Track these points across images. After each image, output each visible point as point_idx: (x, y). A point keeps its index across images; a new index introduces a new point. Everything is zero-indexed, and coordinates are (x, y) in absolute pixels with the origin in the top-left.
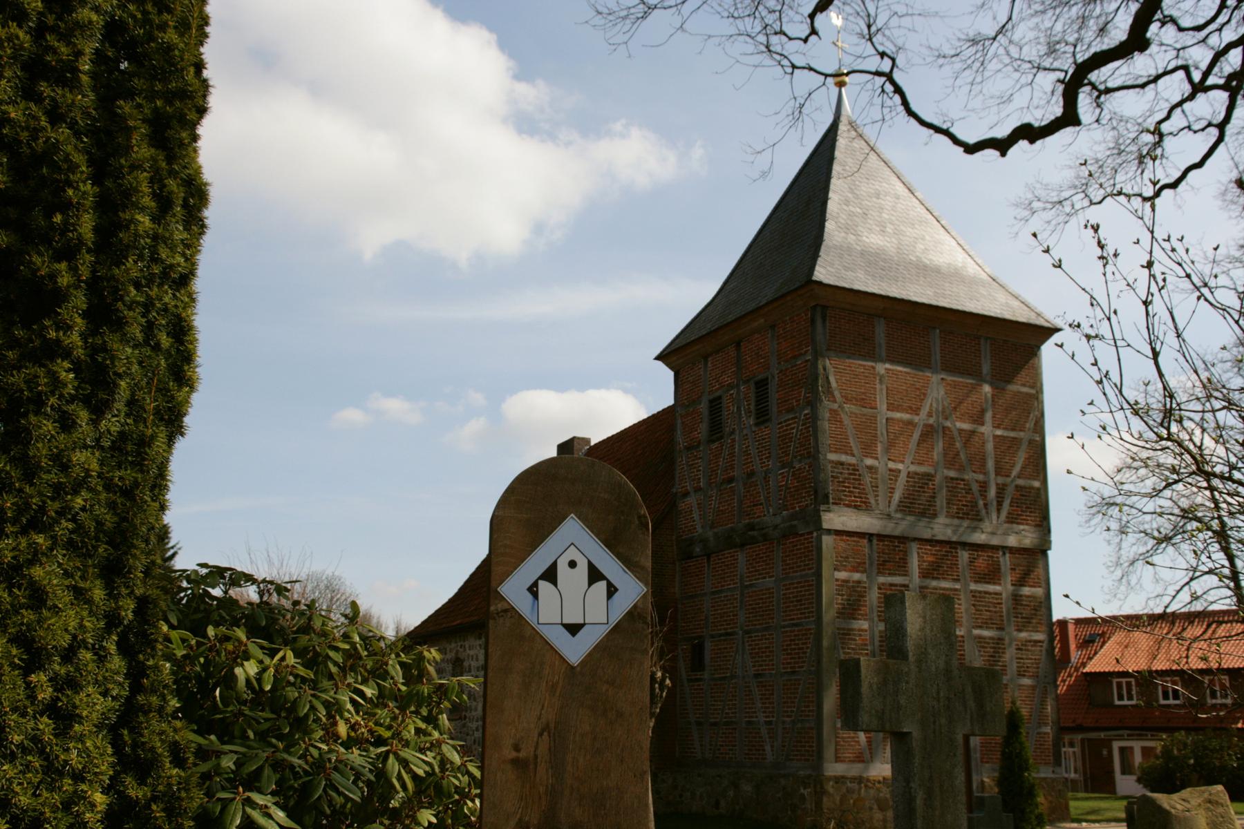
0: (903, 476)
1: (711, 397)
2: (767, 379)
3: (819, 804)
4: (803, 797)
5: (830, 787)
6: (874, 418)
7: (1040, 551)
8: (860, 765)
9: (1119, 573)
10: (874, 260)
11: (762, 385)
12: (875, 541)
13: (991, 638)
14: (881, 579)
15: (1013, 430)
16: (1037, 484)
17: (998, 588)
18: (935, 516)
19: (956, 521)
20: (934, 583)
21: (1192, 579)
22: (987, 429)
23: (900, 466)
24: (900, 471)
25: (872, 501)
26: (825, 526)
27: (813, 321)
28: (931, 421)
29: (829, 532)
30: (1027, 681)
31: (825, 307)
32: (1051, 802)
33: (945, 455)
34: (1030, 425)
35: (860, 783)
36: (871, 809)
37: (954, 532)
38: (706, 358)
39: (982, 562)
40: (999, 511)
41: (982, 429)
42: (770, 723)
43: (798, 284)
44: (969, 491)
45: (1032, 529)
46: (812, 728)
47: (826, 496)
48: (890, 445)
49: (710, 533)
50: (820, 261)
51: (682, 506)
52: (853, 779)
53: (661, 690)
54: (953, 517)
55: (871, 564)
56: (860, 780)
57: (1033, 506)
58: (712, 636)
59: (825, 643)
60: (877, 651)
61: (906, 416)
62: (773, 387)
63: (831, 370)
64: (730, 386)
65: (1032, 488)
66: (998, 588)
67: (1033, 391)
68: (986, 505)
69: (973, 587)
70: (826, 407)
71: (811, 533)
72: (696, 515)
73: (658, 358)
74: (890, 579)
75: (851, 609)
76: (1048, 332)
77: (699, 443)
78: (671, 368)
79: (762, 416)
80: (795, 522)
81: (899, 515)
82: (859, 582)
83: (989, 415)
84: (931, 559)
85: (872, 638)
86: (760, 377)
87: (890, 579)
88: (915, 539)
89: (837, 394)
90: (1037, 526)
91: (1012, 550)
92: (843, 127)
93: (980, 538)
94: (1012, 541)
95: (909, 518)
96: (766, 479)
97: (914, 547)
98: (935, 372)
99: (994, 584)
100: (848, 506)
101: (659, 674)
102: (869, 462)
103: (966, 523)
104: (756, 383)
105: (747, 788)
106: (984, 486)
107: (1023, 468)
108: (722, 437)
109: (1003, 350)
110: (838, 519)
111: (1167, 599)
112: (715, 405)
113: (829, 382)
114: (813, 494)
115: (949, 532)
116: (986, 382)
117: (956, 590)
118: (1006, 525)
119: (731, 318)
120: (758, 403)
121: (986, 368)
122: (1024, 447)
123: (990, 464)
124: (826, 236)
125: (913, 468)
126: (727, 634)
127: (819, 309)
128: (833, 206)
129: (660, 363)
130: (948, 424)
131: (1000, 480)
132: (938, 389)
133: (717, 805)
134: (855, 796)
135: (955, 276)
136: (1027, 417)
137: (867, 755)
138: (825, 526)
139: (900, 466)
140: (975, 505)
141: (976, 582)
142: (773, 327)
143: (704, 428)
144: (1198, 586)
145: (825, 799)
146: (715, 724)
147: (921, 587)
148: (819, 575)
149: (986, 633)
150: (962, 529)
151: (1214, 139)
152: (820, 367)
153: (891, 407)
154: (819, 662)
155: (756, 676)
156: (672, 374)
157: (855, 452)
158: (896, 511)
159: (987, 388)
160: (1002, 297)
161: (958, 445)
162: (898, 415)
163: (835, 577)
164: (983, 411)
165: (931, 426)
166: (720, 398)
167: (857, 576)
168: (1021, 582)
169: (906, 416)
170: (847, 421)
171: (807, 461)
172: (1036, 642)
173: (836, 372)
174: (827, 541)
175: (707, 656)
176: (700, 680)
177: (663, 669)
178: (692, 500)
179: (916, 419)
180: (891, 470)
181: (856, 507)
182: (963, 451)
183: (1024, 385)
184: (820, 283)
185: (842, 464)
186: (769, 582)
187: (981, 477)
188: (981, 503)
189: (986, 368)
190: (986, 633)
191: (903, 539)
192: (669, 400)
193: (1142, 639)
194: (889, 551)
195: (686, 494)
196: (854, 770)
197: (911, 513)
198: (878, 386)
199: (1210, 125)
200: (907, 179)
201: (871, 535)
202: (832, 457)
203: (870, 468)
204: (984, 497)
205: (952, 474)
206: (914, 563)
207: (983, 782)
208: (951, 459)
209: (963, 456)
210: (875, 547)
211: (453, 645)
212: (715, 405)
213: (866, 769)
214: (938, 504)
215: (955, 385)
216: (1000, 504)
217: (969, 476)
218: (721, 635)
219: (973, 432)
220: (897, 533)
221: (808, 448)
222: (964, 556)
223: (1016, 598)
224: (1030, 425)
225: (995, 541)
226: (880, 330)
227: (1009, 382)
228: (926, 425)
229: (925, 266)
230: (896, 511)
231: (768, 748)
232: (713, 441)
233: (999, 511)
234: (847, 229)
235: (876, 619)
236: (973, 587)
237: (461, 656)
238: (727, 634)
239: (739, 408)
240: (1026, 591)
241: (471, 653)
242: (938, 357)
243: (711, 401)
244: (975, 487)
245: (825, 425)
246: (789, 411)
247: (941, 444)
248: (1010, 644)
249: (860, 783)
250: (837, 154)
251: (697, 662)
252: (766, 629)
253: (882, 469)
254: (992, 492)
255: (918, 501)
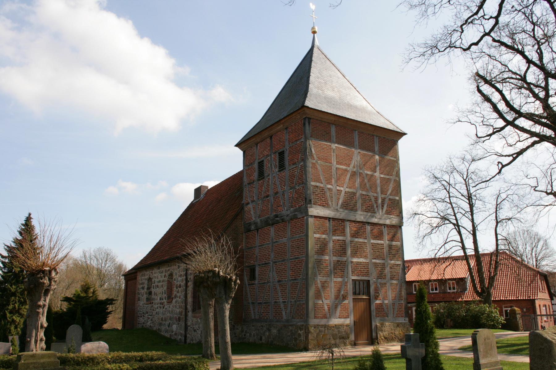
0: (343, 193)
1: (259, 161)
2: (284, 151)
3: (307, 337)
4: (300, 335)
5: (312, 329)
6: (331, 168)
7: (399, 226)
8: (325, 320)
9: (419, 241)
10: (329, 100)
11: (281, 154)
12: (331, 221)
13: (379, 263)
14: (334, 238)
15: (388, 175)
16: (397, 198)
17: (382, 242)
18: (356, 210)
19: (365, 213)
20: (356, 240)
21: (445, 243)
22: (377, 174)
23: (342, 189)
24: (342, 191)
25: (330, 203)
26: (310, 214)
27: (304, 124)
28: (355, 170)
29: (311, 216)
30: (395, 282)
31: (309, 119)
32: (404, 333)
33: (361, 184)
34: (394, 173)
35: (325, 327)
36: (330, 339)
37: (365, 218)
38: (257, 145)
39: (376, 230)
40: (382, 209)
41: (375, 174)
42: (285, 302)
43: (298, 108)
44: (370, 200)
45: (396, 217)
46: (304, 304)
47: (310, 201)
48: (338, 180)
49: (258, 220)
50: (307, 99)
51: (246, 209)
52: (322, 326)
53: (235, 285)
54: (364, 211)
55: (330, 231)
56: (325, 326)
57: (395, 206)
58: (259, 265)
59: (310, 265)
60: (332, 269)
61: (344, 167)
62: (286, 155)
63: (312, 146)
64: (268, 156)
65: (395, 200)
66: (382, 242)
67: (395, 159)
68: (377, 206)
69: (372, 241)
70: (310, 162)
71: (304, 217)
72: (252, 213)
73: (236, 146)
74: (338, 238)
75: (322, 250)
76: (401, 134)
77: (254, 181)
78: (242, 150)
79: (282, 167)
80: (296, 213)
81: (341, 210)
82: (324, 239)
83: (378, 168)
84: (355, 229)
85: (330, 263)
86: (281, 150)
87: (338, 238)
88: (348, 220)
89: (315, 156)
90: (397, 216)
91: (388, 226)
92: (315, 50)
93: (375, 220)
94: (388, 222)
95: (346, 211)
96: (283, 195)
97: (348, 224)
98: (356, 149)
99: (381, 240)
100: (320, 205)
101: (234, 277)
102: (329, 186)
103: (369, 214)
104: (279, 153)
105: (274, 331)
106: (376, 199)
107: (392, 191)
108: (264, 178)
109: (384, 140)
110: (315, 211)
111: (436, 251)
112: (261, 164)
113: (311, 151)
114: (304, 201)
115: (362, 218)
116: (377, 154)
117: (365, 243)
118: (386, 215)
119: (268, 126)
120: (280, 162)
121: (377, 148)
122: (392, 182)
123: (379, 189)
124: (309, 90)
125: (347, 190)
126: (266, 264)
127: (307, 119)
128: (312, 79)
129: (237, 148)
130: (361, 171)
131: (383, 196)
132: (357, 156)
133: (261, 339)
134: (323, 333)
135: (363, 110)
136: (393, 168)
137: (328, 316)
138: (310, 214)
139: (342, 189)
140: (373, 206)
141: (373, 239)
142: (286, 129)
143: (256, 174)
144: (447, 246)
145: (310, 335)
146: (260, 303)
147: (351, 241)
148: (307, 236)
149: (377, 261)
150: (368, 217)
151: (494, 23)
152: (308, 144)
153: (338, 163)
154: (307, 274)
155: (279, 281)
156: (242, 152)
157: (323, 182)
158: (340, 208)
159: (377, 157)
160: (382, 120)
161: (366, 181)
162: (341, 167)
163: (314, 236)
164: (376, 167)
165: (355, 172)
166: (263, 161)
167: (324, 236)
168: (392, 239)
169: (344, 167)
170: (319, 168)
171: (302, 185)
172: (398, 265)
173: (315, 146)
174: (311, 220)
175: (257, 273)
176: (254, 284)
177: (236, 275)
178: (250, 206)
179: (349, 169)
180: (338, 190)
181: (323, 206)
182: (368, 183)
183: (392, 157)
184: (308, 107)
185: (317, 187)
186: (285, 240)
187: (375, 195)
188: (375, 205)
189: (377, 148)
190: (377, 261)
191: (343, 220)
192: (239, 167)
193: (427, 267)
194: (338, 224)
195: (248, 204)
196: (323, 322)
197: (346, 209)
198: (332, 154)
199: (491, 17)
200: (342, 71)
201: (330, 218)
202: (313, 183)
203: (329, 189)
204: (376, 203)
205: (364, 193)
206: (348, 230)
207: (376, 325)
208: (363, 186)
209: (368, 185)
210: (331, 224)
211: (148, 272)
212: (261, 164)
213: (328, 321)
214: (358, 205)
215: (364, 155)
216: (383, 206)
217: (371, 194)
218: (263, 264)
219: (372, 175)
220: (341, 218)
221: (302, 180)
222: (368, 228)
223: (390, 247)
224: (394, 173)
225: (381, 222)
226: (333, 129)
227: (386, 155)
228: (352, 172)
229: (351, 105)
230: (340, 208)
231: (284, 313)
232: (260, 180)
233: (382, 209)
234: (318, 88)
235: (332, 255)
236: (372, 241)
237: (151, 277)
238: (266, 264)
239: (271, 165)
240: (394, 243)
241: (155, 275)
242: (357, 140)
243: (259, 163)
244: (373, 199)
245: (310, 169)
246: (293, 164)
247: (359, 180)
248: (387, 266)
249: (325, 327)
250: (313, 59)
251: (252, 276)
252: (284, 260)
253: (334, 190)
254: (380, 201)
255: (349, 204)
